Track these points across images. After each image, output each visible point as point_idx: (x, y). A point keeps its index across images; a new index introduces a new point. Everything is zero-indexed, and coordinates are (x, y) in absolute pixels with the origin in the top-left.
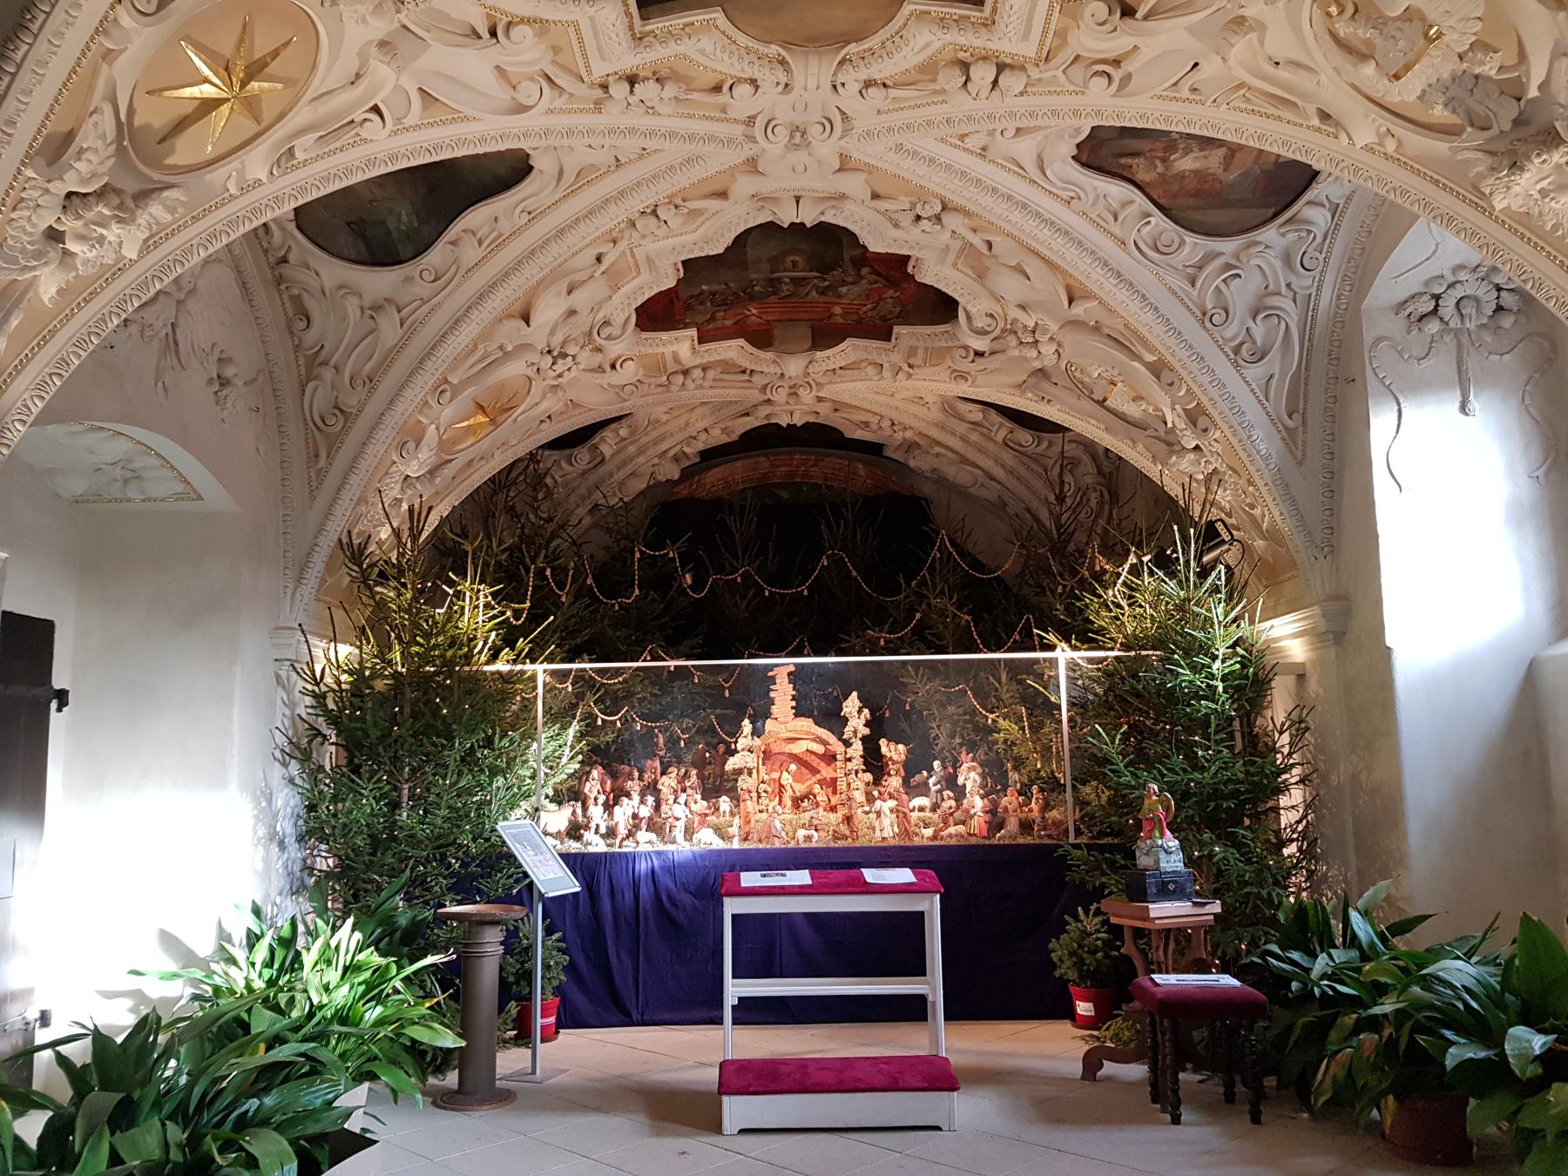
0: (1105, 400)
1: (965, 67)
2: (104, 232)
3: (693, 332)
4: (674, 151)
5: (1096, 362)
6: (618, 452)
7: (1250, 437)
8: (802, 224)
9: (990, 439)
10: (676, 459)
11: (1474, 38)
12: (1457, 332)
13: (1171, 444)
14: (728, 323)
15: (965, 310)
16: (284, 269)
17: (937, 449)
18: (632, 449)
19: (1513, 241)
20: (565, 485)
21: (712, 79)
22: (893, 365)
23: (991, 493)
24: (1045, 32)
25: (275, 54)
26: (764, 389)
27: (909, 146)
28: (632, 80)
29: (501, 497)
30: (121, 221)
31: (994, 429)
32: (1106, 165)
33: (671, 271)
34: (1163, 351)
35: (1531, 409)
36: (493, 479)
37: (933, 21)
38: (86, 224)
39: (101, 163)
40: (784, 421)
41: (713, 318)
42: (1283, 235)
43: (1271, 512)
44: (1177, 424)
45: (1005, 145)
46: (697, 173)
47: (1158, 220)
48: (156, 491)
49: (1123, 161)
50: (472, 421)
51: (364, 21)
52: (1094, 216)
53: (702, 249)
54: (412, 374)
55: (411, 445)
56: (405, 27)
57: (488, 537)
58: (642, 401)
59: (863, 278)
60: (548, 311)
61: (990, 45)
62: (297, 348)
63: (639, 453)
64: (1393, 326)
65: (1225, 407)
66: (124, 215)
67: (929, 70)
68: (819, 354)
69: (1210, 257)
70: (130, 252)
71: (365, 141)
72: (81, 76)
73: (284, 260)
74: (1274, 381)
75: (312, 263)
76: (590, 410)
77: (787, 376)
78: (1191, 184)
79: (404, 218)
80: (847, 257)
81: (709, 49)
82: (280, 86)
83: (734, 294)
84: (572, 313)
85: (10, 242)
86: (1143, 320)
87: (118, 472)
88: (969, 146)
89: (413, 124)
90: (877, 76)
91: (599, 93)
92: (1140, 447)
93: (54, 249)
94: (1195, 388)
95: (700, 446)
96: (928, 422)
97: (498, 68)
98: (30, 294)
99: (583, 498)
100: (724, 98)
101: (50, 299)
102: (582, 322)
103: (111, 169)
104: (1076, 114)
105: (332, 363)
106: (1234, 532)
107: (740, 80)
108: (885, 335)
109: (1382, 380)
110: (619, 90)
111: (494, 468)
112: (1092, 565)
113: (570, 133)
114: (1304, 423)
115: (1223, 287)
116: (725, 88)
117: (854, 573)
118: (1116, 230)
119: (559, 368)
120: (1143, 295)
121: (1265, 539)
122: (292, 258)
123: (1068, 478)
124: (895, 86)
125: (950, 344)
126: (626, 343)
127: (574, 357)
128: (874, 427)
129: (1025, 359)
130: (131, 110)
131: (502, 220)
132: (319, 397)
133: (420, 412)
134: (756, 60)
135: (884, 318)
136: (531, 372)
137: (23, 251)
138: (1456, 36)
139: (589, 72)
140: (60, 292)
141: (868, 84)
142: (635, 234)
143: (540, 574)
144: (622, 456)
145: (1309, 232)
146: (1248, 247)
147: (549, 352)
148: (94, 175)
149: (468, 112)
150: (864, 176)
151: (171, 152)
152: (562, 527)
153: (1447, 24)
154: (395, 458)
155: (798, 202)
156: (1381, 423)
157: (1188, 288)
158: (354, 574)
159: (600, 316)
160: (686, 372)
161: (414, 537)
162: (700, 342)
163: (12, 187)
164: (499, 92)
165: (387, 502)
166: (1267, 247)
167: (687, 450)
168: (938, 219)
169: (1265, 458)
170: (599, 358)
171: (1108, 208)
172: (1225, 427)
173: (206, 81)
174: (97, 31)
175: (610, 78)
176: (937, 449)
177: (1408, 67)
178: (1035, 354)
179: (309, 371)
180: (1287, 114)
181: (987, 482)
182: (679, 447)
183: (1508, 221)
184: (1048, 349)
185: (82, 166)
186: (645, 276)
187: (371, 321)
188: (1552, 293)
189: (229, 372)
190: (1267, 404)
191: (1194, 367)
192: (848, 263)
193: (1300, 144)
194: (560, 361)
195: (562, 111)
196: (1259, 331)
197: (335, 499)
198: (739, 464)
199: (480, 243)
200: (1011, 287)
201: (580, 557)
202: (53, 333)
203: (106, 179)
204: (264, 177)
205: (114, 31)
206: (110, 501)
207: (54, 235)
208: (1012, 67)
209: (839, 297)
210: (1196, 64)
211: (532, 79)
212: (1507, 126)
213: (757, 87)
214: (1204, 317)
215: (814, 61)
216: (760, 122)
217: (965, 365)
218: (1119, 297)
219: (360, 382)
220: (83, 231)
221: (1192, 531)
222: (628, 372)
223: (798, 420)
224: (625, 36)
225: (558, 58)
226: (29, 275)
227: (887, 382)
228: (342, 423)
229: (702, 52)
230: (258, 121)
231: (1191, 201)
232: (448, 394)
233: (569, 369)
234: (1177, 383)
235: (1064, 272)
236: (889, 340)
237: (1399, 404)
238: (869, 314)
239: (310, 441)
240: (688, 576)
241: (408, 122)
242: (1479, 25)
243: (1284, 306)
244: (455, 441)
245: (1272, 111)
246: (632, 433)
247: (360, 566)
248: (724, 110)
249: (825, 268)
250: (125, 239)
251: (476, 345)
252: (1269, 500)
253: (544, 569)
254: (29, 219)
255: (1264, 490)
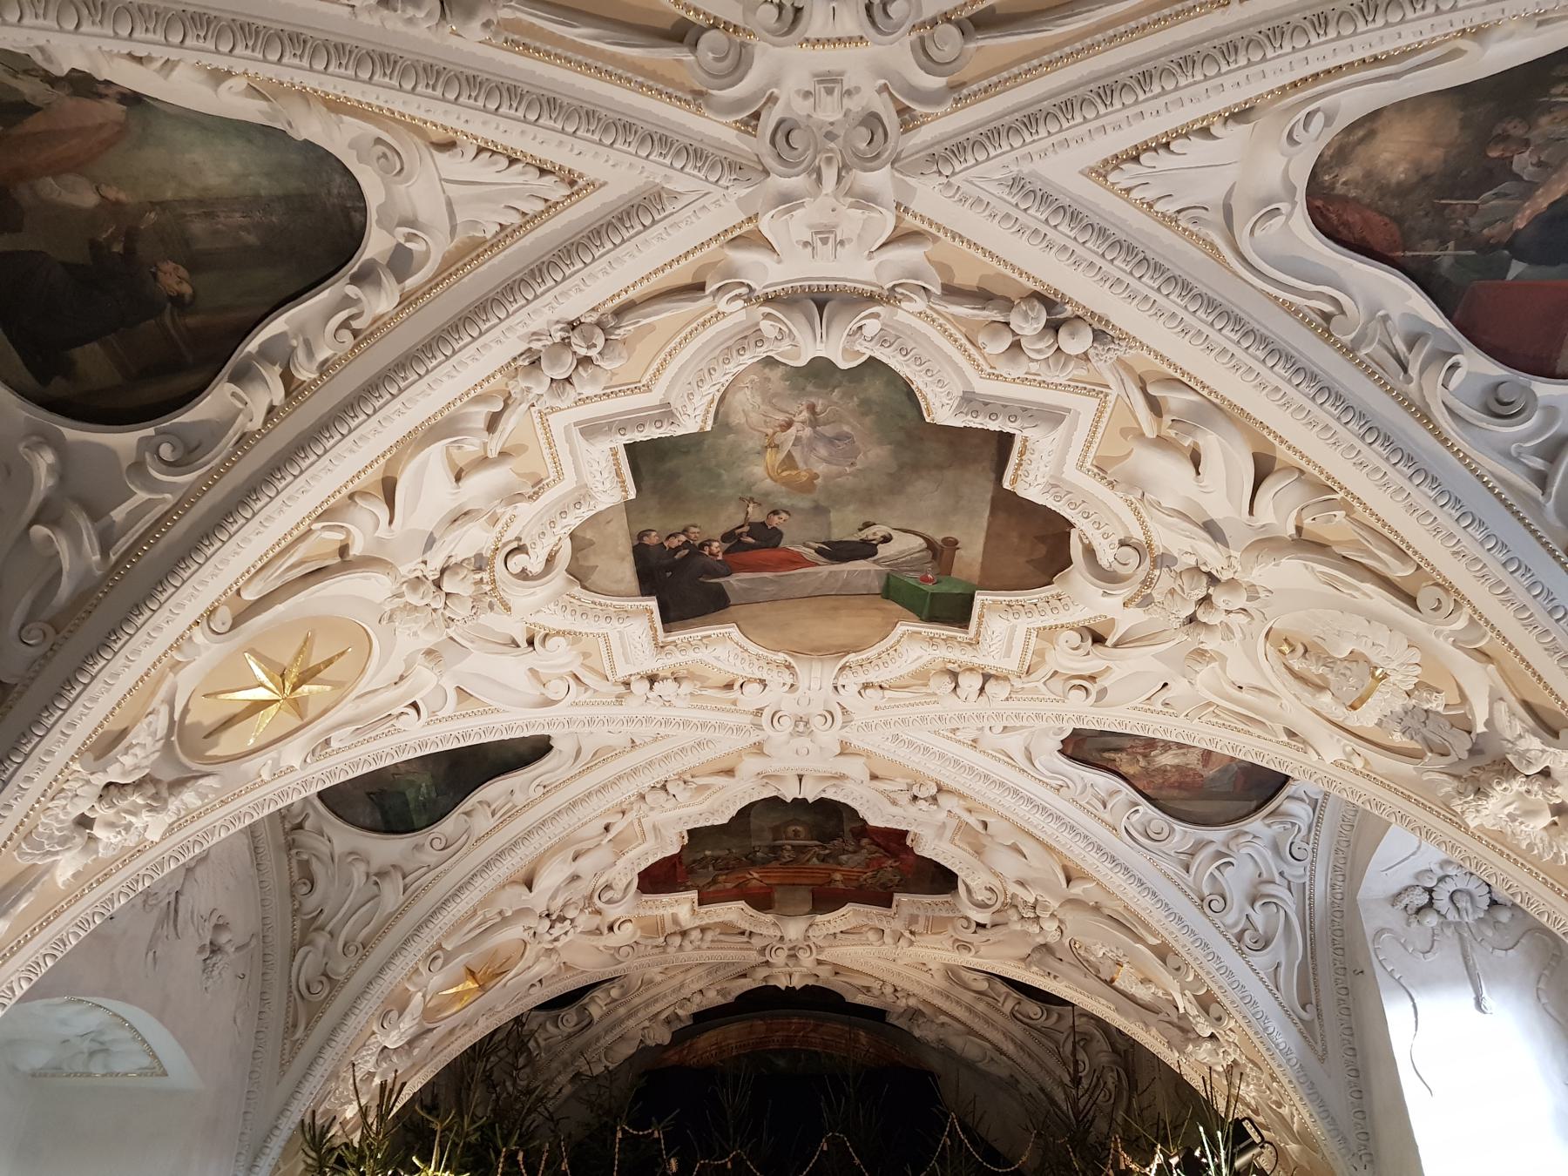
0: (1113, 980)
1: (954, 675)
2: (133, 819)
3: (694, 895)
4: (687, 737)
5: (1101, 944)
6: (608, 1014)
7: (1266, 1029)
8: (805, 800)
9: (998, 1010)
10: (668, 1021)
11: (1417, 680)
12: (1457, 925)
13: (1184, 1031)
14: (729, 886)
15: (967, 886)
16: (299, 836)
17: (943, 1019)
18: (622, 1011)
19: (1493, 856)
20: (548, 1049)
21: (726, 679)
22: (893, 931)
23: (1001, 1070)
24: (1025, 651)
25: (329, 662)
26: (762, 951)
27: (905, 737)
28: (652, 679)
29: (480, 1066)
30: (152, 809)
31: (1001, 1000)
32: (1090, 759)
33: (676, 839)
34: (1166, 935)
35: (1551, 1010)
36: (473, 1047)
37: (924, 639)
38: (118, 813)
39: (147, 757)
40: (782, 983)
41: (714, 882)
42: (1269, 826)
43: (1299, 1112)
44: (1189, 1010)
45: (993, 739)
46: (707, 754)
47: (1145, 808)
48: (119, 1066)
49: (1106, 755)
50: (460, 988)
51: (415, 634)
52: (1083, 803)
53: (707, 819)
54: (407, 942)
55: (394, 1014)
56: (451, 638)
57: (460, 1115)
58: (637, 963)
59: (863, 848)
60: (550, 878)
61: (975, 660)
62: (296, 912)
63: (630, 1015)
64: (1393, 918)
65: (1236, 996)
66: (157, 803)
67: (922, 676)
68: (819, 918)
69: (1200, 845)
70: (154, 835)
71: (399, 731)
72: (148, 682)
73: (300, 826)
74: (1282, 970)
75: (327, 830)
76: (583, 972)
77: (786, 939)
78: (1174, 778)
79: (424, 790)
80: (847, 829)
81: (724, 656)
82: (328, 688)
83: (736, 859)
84: (575, 878)
85: (40, 829)
86: (1142, 904)
87: (86, 1045)
88: (961, 738)
89: (446, 715)
90: (874, 680)
91: (622, 689)
92: (1154, 1031)
93: (81, 836)
94: (1203, 975)
95: (694, 1008)
96: (932, 991)
97: (531, 670)
98: (46, 878)
99: (566, 1065)
100: (735, 693)
101: (64, 882)
102: (583, 887)
103: (153, 763)
104: (1058, 717)
105: (328, 928)
106: (1264, 1132)
107: (750, 680)
108: (887, 902)
109: (1391, 974)
110: (640, 687)
111: (476, 1036)
112: (1117, 1161)
113: (591, 722)
114: (1319, 1016)
115: (1217, 873)
116: (737, 686)
117: (857, 1161)
118: (1106, 816)
119: (556, 932)
120: (1140, 880)
121: (1298, 1142)
122: (307, 825)
123: (1082, 1056)
124: (890, 688)
125: (951, 915)
126: (628, 907)
127: (572, 921)
128: (877, 993)
129: (1027, 934)
130: (186, 711)
131: (517, 794)
132: (309, 964)
133: (409, 979)
134: (765, 665)
135: (883, 885)
136: (527, 936)
137: (50, 837)
138: (1400, 677)
139: (613, 668)
140: (75, 876)
141: (866, 686)
142: (644, 806)
143: (512, 1157)
144: (613, 1017)
145: (1293, 824)
146: (1237, 836)
147: (548, 915)
148: (136, 767)
149: (495, 705)
150: (862, 760)
151: (215, 745)
152: (540, 1099)
153: (1391, 666)
154: (375, 1028)
155: (800, 780)
156: (1397, 1014)
157: (1183, 873)
158: (310, 1161)
159: (602, 881)
160: (684, 934)
161: (381, 1118)
162: (700, 904)
163: (56, 780)
164: (532, 691)
165: (359, 1075)
166: (1255, 837)
167: (680, 1012)
168: (934, 799)
169: (1286, 1053)
170: (597, 920)
171: (1096, 796)
172: (1239, 1018)
173: (261, 685)
174: (171, 647)
175: (633, 678)
176: (943, 1019)
177: (1362, 700)
178: (1037, 930)
179: (304, 933)
180: (1256, 731)
181: (996, 1055)
182: (672, 1008)
183: (1485, 838)
184: (1051, 926)
185: (128, 760)
186: (650, 843)
187: (375, 888)
188: (1542, 908)
189: (223, 938)
190: (1278, 995)
191: (1199, 953)
192: (848, 836)
193: (1273, 756)
194: (558, 925)
195: (586, 704)
196: (1258, 917)
197: (305, 1075)
198: (734, 1027)
199: (493, 814)
200: (1009, 866)
201: (557, 1136)
202: (57, 914)
203: (147, 771)
204: (297, 764)
205: (186, 647)
206: (68, 1075)
207: (84, 822)
208: (996, 678)
209: (840, 864)
210: (1165, 685)
211: (561, 678)
212: (1465, 755)
213: (765, 686)
214: (1203, 903)
215: (817, 667)
216: (767, 714)
217: (967, 936)
218: (1116, 880)
219: (352, 948)
220: (113, 819)
221: (1219, 1134)
222: (625, 934)
223: (797, 983)
224: (649, 646)
225: (587, 662)
226: (49, 860)
227: (888, 947)
228: (327, 992)
229: (717, 658)
230: (302, 719)
231: (1175, 793)
232: (440, 961)
233: (566, 933)
234: (1184, 968)
235: (1059, 853)
236: (890, 907)
237: (1412, 1000)
238: (869, 881)
239: (291, 1010)
240: (673, 1161)
241: (440, 715)
242: (1418, 671)
243: (1280, 895)
244: (439, 1009)
245: (1241, 726)
246: (623, 995)
247: (318, 1151)
248: (734, 703)
249: (825, 837)
250: (152, 825)
251: (475, 911)
252: (1296, 1098)
253: (516, 1153)
254: (64, 807)
255: (1288, 1087)
